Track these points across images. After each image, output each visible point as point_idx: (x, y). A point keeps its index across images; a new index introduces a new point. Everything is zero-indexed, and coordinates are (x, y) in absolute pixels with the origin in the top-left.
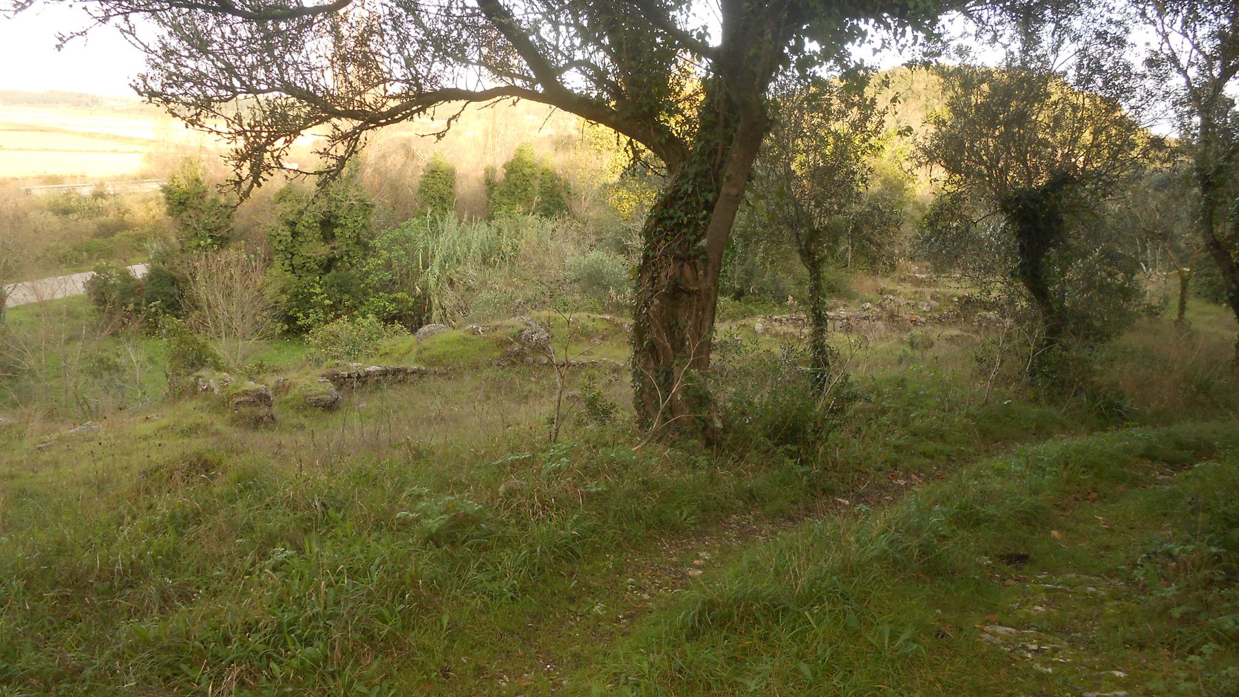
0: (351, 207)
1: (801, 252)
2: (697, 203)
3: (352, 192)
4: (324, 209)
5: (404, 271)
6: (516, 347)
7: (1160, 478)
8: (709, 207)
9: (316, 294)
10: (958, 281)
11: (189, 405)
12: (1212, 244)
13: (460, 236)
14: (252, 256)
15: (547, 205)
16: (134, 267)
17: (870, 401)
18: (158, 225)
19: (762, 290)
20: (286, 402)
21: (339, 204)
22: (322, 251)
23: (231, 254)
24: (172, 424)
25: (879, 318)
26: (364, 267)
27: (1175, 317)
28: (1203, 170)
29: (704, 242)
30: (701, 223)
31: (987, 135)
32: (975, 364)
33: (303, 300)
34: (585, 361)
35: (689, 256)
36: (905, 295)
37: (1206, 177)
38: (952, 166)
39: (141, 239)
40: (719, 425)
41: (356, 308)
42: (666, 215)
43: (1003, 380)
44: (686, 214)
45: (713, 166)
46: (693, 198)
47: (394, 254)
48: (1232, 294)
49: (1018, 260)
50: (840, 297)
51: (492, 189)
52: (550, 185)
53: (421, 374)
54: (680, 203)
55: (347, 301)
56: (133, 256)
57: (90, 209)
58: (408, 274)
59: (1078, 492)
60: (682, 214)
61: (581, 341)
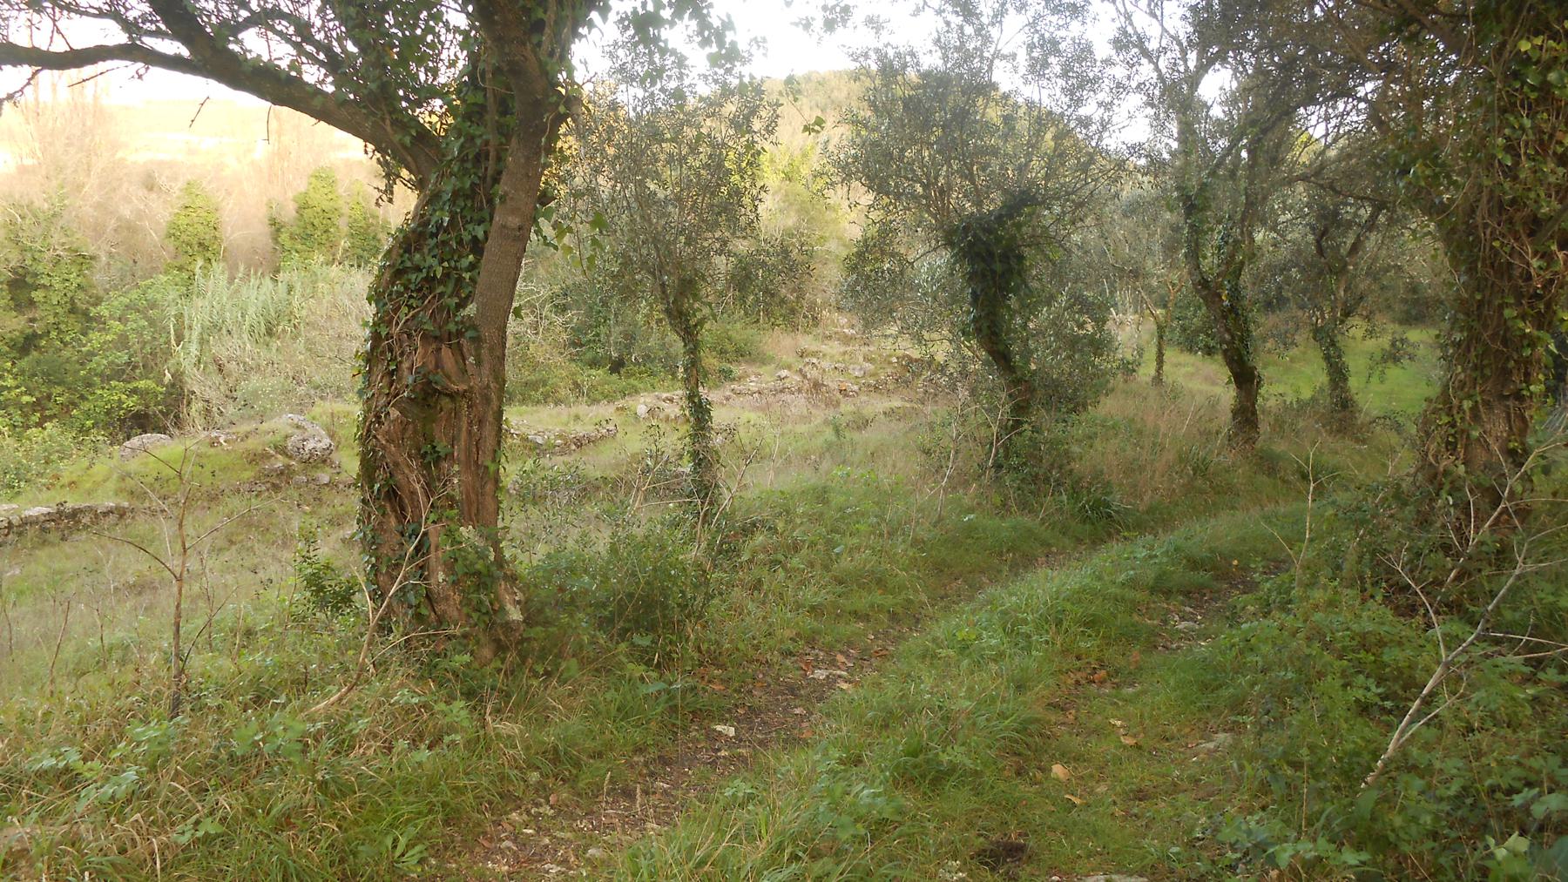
0: (57, 261)
1: (668, 312)
2: (460, 242)
3: (57, 238)
6: (280, 462)
7: (1182, 625)
8: (477, 247)
12: (1200, 283)
15: (359, 251)
17: (776, 532)
25: (799, 391)
27: (1153, 372)
28: (1184, 189)
29: (471, 309)
30: (467, 276)
32: (921, 458)
35: (450, 333)
36: (832, 357)
37: (1189, 198)
38: (877, 184)
40: (515, 615)
41: (75, 405)
42: (408, 264)
43: (961, 481)
44: (442, 261)
45: (483, 179)
46: (453, 235)
48: (1225, 346)
50: (752, 362)
51: (278, 230)
52: (362, 224)
54: (432, 242)
55: (60, 395)
60: (434, 262)
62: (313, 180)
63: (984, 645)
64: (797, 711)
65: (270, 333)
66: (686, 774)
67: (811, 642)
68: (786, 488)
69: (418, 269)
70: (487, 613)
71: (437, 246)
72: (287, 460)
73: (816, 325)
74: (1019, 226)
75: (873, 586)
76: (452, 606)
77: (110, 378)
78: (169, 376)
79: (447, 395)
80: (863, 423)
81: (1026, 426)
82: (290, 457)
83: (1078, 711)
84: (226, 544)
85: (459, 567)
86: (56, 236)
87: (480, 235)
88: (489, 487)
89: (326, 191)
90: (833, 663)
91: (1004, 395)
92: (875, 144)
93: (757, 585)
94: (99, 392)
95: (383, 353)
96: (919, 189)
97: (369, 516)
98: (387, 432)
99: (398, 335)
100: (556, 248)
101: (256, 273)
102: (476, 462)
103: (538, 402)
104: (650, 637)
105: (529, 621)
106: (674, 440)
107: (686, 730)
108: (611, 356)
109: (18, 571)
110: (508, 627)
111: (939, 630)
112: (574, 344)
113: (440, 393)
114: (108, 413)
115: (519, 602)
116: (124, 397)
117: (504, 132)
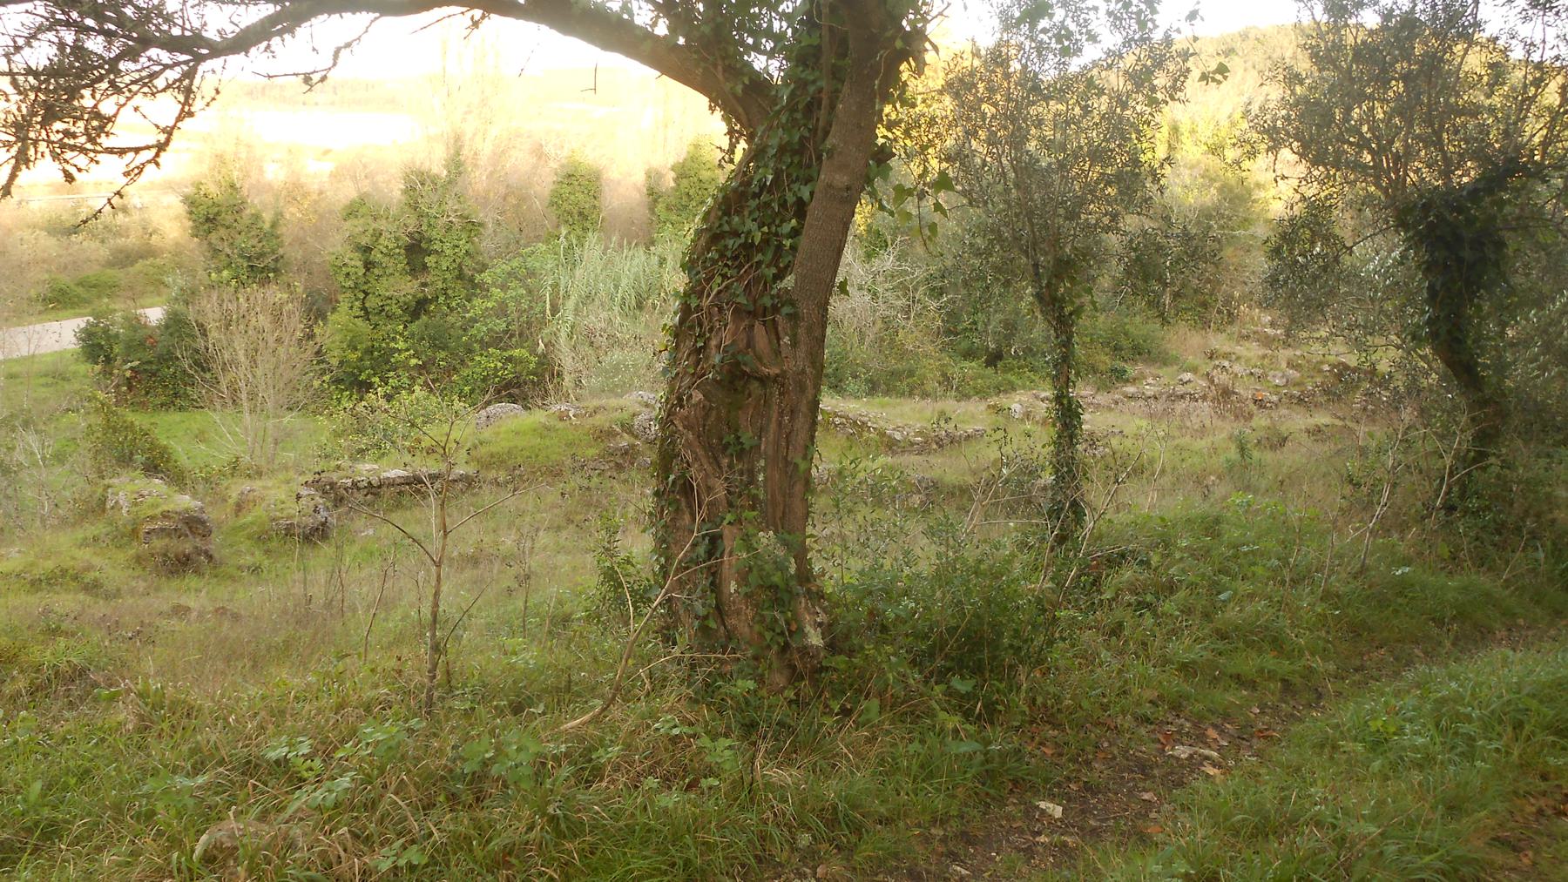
0: (449, 227)
2: (783, 205)
3: (451, 204)
6: (625, 441)
8: (801, 209)
10: (1325, 341)
13: (605, 268)
18: (178, 251)
19: (1029, 351)
21: (432, 221)
22: (407, 288)
25: (1204, 398)
29: (789, 281)
30: (787, 243)
31: (1371, 98)
36: (1248, 360)
38: (1315, 152)
40: (815, 639)
42: (726, 228)
43: (1394, 523)
45: (814, 131)
49: (1423, 312)
51: (655, 201)
54: (753, 203)
57: (106, 227)
59: (1544, 794)
60: (752, 226)
63: (1407, 743)
64: (1146, 796)
65: (640, 306)
66: (992, 859)
67: (1176, 708)
68: (1169, 516)
69: (736, 234)
70: (782, 633)
71: (758, 208)
72: (632, 440)
73: (1231, 323)
74: (1501, 204)
75: (1266, 646)
76: (743, 623)
77: (488, 345)
79: (756, 378)
80: (1279, 441)
81: (1492, 460)
82: (636, 437)
83: (1537, 852)
84: (563, 524)
85: (753, 578)
86: (450, 202)
87: (806, 196)
88: (799, 487)
90: (1202, 739)
91: (1464, 419)
92: (1306, 100)
93: (1116, 630)
94: (478, 358)
95: (691, 328)
96: (1367, 158)
97: (662, 511)
98: (686, 418)
99: (709, 307)
100: (892, 214)
102: (785, 458)
103: (903, 394)
104: (973, 682)
105: (832, 647)
106: (1038, 442)
107: (1002, 802)
108: (988, 348)
109: (371, 532)
110: (805, 651)
111: (1346, 714)
112: (948, 332)
113: (749, 376)
114: (484, 380)
115: (820, 625)
116: (500, 365)
117: (836, 74)
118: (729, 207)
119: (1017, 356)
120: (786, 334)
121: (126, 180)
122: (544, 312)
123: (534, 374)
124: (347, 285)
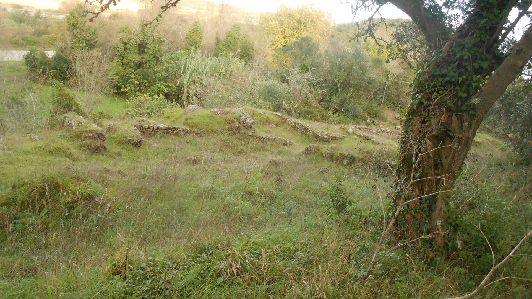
3: (155, 33)
4: (141, 39)
5: (174, 73)
6: (237, 125)
9: (132, 78)
11: (56, 134)
14: (105, 55)
15: (242, 54)
16: (48, 52)
20: (113, 138)
22: (137, 58)
23: (95, 52)
24: (44, 146)
26: (156, 69)
33: (126, 80)
34: (269, 137)
39: (54, 40)
41: (149, 87)
47: (170, 65)
53: (187, 132)
56: (49, 47)
58: (175, 75)
61: (266, 125)
62: (233, 27)
72: (239, 124)
78: (178, 83)
89: (237, 32)
94: (157, 84)
101: (211, 55)
116: (164, 87)
118: (439, 65)
119: (343, 112)
120: (467, 122)
121: (161, 10)
122: (180, 73)
123: (175, 92)
124: (118, 54)
